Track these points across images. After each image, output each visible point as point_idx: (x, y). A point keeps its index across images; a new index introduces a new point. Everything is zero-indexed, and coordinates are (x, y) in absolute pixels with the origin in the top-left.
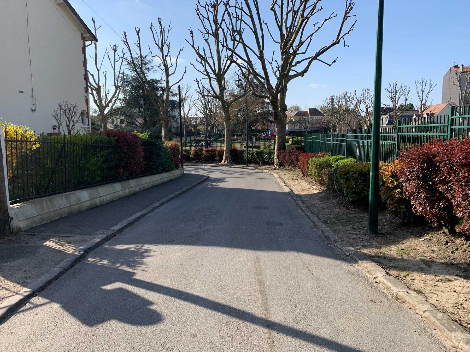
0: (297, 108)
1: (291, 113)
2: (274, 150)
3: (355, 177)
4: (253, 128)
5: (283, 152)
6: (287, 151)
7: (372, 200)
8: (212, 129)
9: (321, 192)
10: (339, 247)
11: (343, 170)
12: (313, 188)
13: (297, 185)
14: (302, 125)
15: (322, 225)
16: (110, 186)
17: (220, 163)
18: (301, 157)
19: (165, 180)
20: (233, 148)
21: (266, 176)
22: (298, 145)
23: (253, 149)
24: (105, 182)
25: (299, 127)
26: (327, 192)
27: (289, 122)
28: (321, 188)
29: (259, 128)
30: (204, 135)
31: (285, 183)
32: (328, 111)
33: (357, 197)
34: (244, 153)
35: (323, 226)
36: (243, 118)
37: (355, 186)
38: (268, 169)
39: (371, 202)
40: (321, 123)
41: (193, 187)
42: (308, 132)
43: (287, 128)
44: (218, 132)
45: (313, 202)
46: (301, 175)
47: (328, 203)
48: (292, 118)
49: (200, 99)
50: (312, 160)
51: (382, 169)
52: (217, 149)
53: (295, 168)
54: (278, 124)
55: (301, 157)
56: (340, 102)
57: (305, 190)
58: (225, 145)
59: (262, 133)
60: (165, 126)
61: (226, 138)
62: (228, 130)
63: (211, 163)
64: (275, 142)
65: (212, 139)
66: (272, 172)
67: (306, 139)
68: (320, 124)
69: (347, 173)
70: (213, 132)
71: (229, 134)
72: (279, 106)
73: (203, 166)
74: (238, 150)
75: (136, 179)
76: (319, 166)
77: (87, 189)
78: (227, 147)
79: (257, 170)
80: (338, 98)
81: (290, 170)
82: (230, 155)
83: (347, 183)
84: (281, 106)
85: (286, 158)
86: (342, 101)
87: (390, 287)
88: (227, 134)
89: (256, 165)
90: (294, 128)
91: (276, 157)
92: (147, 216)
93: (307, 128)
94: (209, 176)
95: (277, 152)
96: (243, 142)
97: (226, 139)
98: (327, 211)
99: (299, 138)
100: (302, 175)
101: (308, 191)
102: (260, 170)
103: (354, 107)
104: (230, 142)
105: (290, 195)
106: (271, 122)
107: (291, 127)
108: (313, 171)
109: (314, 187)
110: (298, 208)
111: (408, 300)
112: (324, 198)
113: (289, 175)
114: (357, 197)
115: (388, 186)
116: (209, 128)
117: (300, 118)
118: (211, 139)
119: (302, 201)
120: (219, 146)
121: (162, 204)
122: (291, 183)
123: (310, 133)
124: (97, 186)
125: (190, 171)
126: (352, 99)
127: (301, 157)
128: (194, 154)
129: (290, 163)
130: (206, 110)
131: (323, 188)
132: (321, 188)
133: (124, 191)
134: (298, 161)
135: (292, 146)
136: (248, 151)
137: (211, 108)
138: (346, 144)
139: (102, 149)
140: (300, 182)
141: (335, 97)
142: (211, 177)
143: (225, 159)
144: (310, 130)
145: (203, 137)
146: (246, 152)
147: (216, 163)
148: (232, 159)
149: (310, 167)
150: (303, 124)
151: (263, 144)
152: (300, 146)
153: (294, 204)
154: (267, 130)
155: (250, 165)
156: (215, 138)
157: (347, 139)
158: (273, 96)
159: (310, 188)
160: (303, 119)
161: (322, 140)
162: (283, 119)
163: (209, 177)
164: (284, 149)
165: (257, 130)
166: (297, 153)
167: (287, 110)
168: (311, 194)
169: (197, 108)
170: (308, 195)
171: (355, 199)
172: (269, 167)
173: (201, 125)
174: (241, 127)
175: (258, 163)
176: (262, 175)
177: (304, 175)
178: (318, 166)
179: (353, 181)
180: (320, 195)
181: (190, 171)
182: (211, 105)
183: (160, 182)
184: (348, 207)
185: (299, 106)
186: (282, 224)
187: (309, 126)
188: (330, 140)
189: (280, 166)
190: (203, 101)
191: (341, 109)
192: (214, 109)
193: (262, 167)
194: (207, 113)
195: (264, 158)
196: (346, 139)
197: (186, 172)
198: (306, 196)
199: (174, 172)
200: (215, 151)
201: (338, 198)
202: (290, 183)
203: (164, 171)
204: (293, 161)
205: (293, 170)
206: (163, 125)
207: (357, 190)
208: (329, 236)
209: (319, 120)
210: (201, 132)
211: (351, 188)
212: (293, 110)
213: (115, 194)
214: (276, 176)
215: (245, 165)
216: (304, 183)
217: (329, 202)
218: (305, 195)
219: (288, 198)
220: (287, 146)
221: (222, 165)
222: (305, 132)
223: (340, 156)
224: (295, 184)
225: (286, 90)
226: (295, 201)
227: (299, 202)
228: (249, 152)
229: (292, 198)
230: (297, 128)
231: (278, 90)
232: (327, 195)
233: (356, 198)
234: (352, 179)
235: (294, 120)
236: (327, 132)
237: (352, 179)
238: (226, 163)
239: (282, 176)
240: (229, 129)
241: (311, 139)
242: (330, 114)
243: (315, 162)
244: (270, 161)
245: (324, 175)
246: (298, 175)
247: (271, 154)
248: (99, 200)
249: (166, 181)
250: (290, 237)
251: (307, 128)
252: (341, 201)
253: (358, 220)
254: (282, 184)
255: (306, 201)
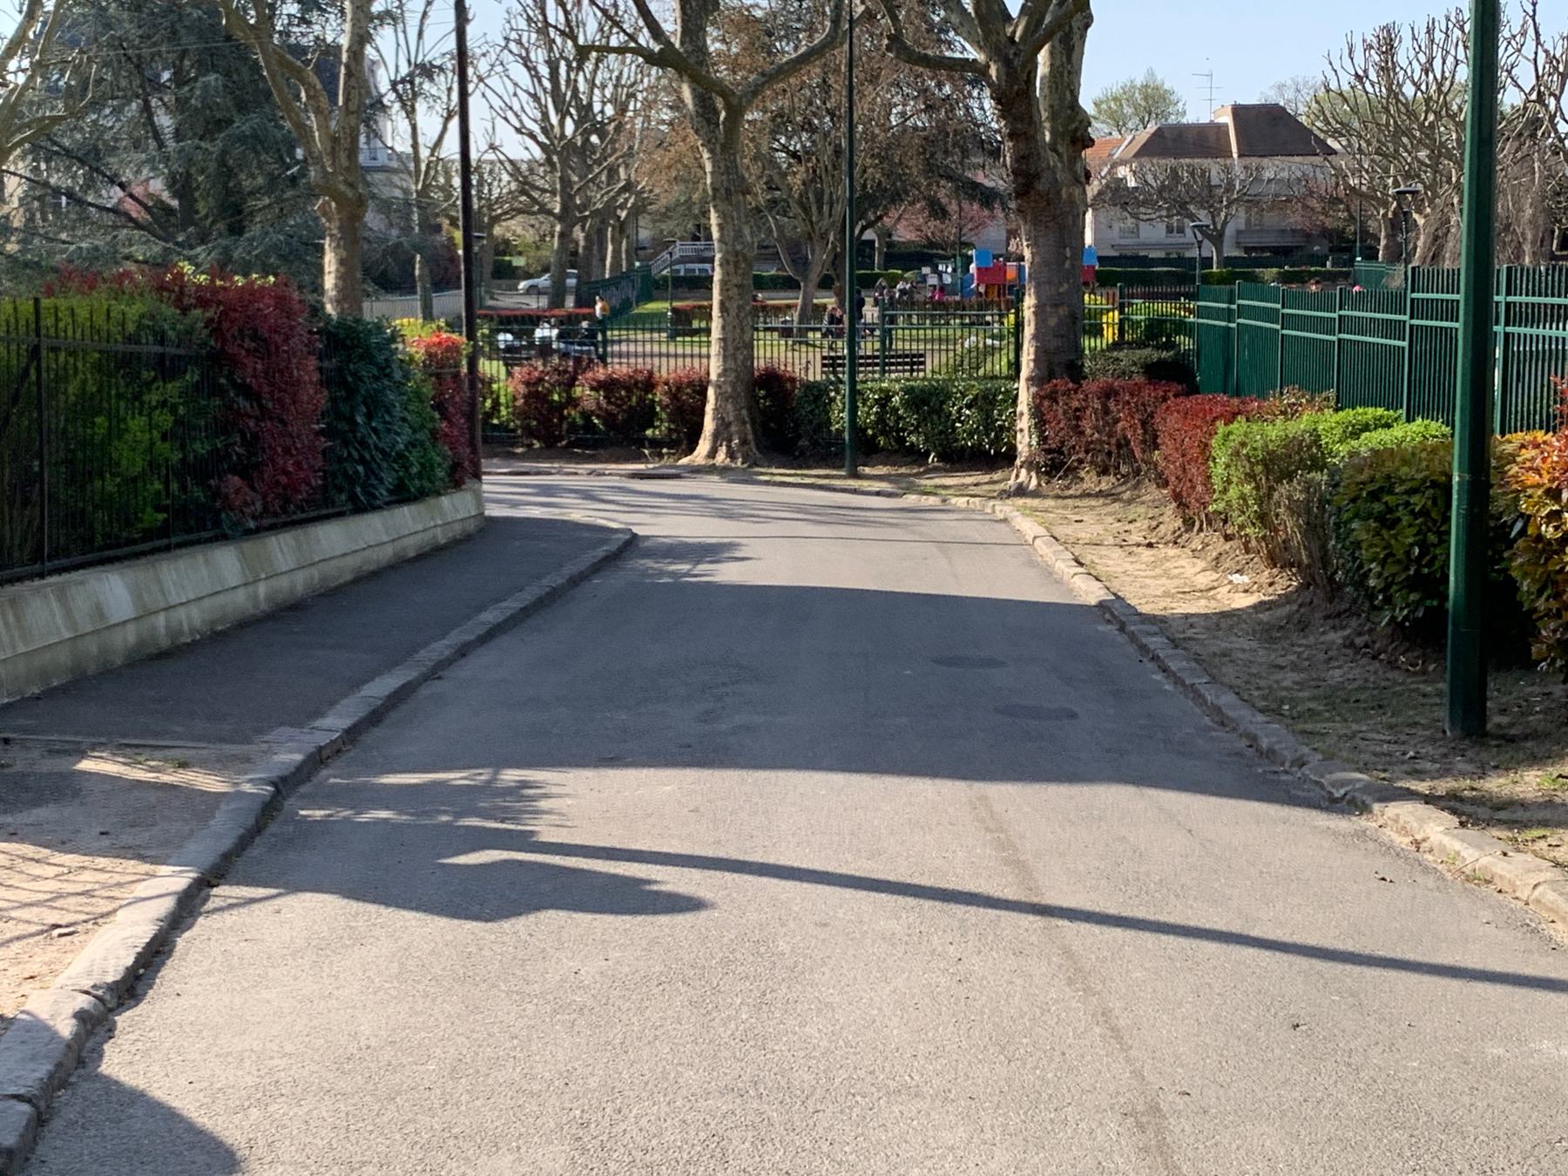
0: (1153, 99)
1: (1116, 134)
2: (1017, 377)
3: (1417, 509)
4: (869, 235)
5: (1067, 393)
6: (1090, 386)
7: (1461, 590)
8: (596, 239)
9: (1271, 602)
10: (1312, 777)
11: (1363, 477)
12: (1231, 582)
13: (1148, 573)
14: (1192, 217)
15: (1253, 715)
16: (200, 558)
17: (685, 461)
18: (1173, 421)
19: (411, 545)
20: (760, 364)
21: (971, 531)
22: (1158, 348)
23: (883, 372)
24: (174, 540)
25: (1170, 230)
26: (1307, 596)
27: (1100, 193)
28: (1271, 584)
29: (904, 234)
30: (544, 281)
31: (1081, 564)
32: (1356, 125)
33: (1428, 603)
34: (833, 400)
35: (1255, 721)
36: (807, 171)
37: (1417, 550)
38: (976, 490)
39: (1455, 596)
40: (1314, 203)
41: (575, 581)
42: (1227, 262)
43: (1089, 239)
44: (630, 264)
45: (1224, 645)
46: (1171, 521)
47: (1300, 646)
48: (1122, 172)
49: (519, 42)
50: (1230, 433)
51: (1519, 459)
52: (664, 374)
53: (1136, 487)
54: (1036, 222)
55: (1173, 421)
56: (1437, 64)
57: (1188, 596)
58: (715, 349)
59: (926, 270)
60: (340, 228)
61: (722, 304)
62: (732, 259)
63: (627, 460)
64: (1019, 325)
65: (598, 307)
66: (1003, 508)
67: (1201, 313)
68: (1305, 207)
69: (1381, 489)
70: (603, 260)
71: (736, 280)
72: (1044, 115)
73: (578, 475)
74: (793, 380)
75: (293, 533)
76: (1266, 466)
77: (101, 568)
78: (725, 358)
79: (911, 500)
80: (1423, 38)
81: (1107, 496)
82: (744, 412)
83: (1383, 539)
84: (1053, 117)
85: (1087, 426)
86: (1450, 60)
87: (1458, 853)
88: (724, 283)
89: (903, 470)
90: (1135, 232)
91: (1024, 423)
92: (424, 692)
93: (1221, 234)
94: (636, 530)
95: (1033, 389)
96: (803, 332)
97: (724, 308)
98: (1289, 678)
99: (1163, 308)
100: (1179, 523)
101: (1203, 602)
102: (932, 501)
103: (1528, 101)
104: (742, 331)
105: (1107, 616)
106: (988, 197)
107: (1116, 226)
108: (1233, 492)
109: (1236, 578)
110: (1151, 666)
111: (1500, 872)
112: (1282, 627)
113: (1100, 522)
114: (1428, 603)
115: (1539, 538)
116: (579, 234)
117: (1174, 170)
118: (594, 307)
119: (1168, 638)
120: (676, 356)
121: (463, 652)
122: (1113, 561)
123: (1240, 272)
124: (152, 552)
125: (514, 505)
126: (1510, 50)
127: (1169, 422)
128: (520, 402)
129: (1109, 454)
130: (554, 119)
131: (1285, 583)
132: (1271, 584)
133: (250, 589)
134: (1152, 443)
135: (1121, 355)
136: (858, 387)
137: (590, 105)
138: (1405, 344)
139: (167, 368)
140: (1167, 558)
141: (1406, 34)
142: (648, 537)
143: (716, 436)
144: (1238, 245)
145: (531, 291)
146: (845, 389)
147: (661, 456)
148: (755, 432)
149: (1218, 471)
150: (1192, 207)
151: (933, 340)
152: (1164, 354)
153: (1132, 649)
154: (957, 250)
155: (867, 470)
156: (615, 302)
157: (1412, 317)
158: (1007, 63)
159: (1215, 584)
160: (1192, 174)
161: (1287, 321)
162: (1070, 195)
163: (635, 536)
164: (1075, 371)
165: (890, 245)
166: (1149, 394)
167: (1091, 143)
168: (1221, 613)
169: (497, 103)
170: (1206, 616)
171: (1420, 614)
172: (986, 478)
173: (520, 212)
174: (795, 226)
175: (916, 457)
176: (946, 526)
177: (1184, 522)
178: (1257, 463)
179: (1410, 525)
180: (1264, 617)
181: (514, 505)
182: (592, 84)
183: (386, 554)
184: (1397, 660)
185: (1166, 87)
186: (1073, 716)
187: (1237, 220)
188: (1325, 326)
189: (1046, 473)
190: (539, 56)
191: (1438, 114)
192: (610, 110)
193: (938, 481)
194: (563, 135)
195: (954, 429)
196: (1406, 318)
197: (493, 511)
198: (1190, 620)
199: (445, 501)
200: (649, 384)
201: (1354, 623)
202: (1110, 562)
203: (403, 495)
204: (1123, 444)
205: (1126, 496)
206: (334, 227)
207: (1426, 571)
208: (1277, 747)
209: (1299, 180)
210: (519, 262)
211: (1399, 562)
212: (1128, 110)
213: (221, 599)
214: (1028, 527)
215: (840, 467)
216: (1182, 562)
217: (1304, 642)
218: (1187, 616)
219: (1100, 628)
220: (1093, 358)
221: (696, 471)
222: (1207, 262)
223: (1371, 413)
224: (1138, 566)
225: (1088, 21)
226: (1133, 637)
227: (1156, 642)
228: (861, 393)
229: (1118, 627)
230: (1153, 235)
231: (1040, 21)
232: (1298, 611)
233: (1427, 609)
234: (1405, 520)
235: (1132, 183)
236: (1351, 262)
237: (1405, 520)
238: (721, 457)
239: (1060, 531)
240: (737, 254)
241: (1229, 315)
242: (1369, 143)
243: (1243, 444)
244: (991, 444)
245: (1289, 508)
246: (1154, 523)
247: (992, 401)
248: (167, 627)
249: (412, 554)
250: (1108, 751)
251: (1217, 238)
252: (1366, 638)
253: (1422, 700)
254: (1064, 567)
255: (1190, 639)
